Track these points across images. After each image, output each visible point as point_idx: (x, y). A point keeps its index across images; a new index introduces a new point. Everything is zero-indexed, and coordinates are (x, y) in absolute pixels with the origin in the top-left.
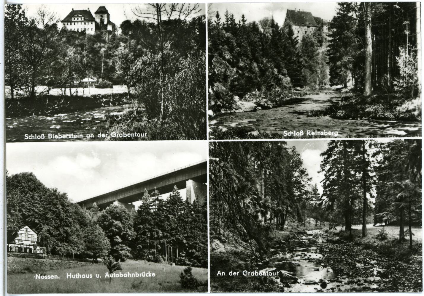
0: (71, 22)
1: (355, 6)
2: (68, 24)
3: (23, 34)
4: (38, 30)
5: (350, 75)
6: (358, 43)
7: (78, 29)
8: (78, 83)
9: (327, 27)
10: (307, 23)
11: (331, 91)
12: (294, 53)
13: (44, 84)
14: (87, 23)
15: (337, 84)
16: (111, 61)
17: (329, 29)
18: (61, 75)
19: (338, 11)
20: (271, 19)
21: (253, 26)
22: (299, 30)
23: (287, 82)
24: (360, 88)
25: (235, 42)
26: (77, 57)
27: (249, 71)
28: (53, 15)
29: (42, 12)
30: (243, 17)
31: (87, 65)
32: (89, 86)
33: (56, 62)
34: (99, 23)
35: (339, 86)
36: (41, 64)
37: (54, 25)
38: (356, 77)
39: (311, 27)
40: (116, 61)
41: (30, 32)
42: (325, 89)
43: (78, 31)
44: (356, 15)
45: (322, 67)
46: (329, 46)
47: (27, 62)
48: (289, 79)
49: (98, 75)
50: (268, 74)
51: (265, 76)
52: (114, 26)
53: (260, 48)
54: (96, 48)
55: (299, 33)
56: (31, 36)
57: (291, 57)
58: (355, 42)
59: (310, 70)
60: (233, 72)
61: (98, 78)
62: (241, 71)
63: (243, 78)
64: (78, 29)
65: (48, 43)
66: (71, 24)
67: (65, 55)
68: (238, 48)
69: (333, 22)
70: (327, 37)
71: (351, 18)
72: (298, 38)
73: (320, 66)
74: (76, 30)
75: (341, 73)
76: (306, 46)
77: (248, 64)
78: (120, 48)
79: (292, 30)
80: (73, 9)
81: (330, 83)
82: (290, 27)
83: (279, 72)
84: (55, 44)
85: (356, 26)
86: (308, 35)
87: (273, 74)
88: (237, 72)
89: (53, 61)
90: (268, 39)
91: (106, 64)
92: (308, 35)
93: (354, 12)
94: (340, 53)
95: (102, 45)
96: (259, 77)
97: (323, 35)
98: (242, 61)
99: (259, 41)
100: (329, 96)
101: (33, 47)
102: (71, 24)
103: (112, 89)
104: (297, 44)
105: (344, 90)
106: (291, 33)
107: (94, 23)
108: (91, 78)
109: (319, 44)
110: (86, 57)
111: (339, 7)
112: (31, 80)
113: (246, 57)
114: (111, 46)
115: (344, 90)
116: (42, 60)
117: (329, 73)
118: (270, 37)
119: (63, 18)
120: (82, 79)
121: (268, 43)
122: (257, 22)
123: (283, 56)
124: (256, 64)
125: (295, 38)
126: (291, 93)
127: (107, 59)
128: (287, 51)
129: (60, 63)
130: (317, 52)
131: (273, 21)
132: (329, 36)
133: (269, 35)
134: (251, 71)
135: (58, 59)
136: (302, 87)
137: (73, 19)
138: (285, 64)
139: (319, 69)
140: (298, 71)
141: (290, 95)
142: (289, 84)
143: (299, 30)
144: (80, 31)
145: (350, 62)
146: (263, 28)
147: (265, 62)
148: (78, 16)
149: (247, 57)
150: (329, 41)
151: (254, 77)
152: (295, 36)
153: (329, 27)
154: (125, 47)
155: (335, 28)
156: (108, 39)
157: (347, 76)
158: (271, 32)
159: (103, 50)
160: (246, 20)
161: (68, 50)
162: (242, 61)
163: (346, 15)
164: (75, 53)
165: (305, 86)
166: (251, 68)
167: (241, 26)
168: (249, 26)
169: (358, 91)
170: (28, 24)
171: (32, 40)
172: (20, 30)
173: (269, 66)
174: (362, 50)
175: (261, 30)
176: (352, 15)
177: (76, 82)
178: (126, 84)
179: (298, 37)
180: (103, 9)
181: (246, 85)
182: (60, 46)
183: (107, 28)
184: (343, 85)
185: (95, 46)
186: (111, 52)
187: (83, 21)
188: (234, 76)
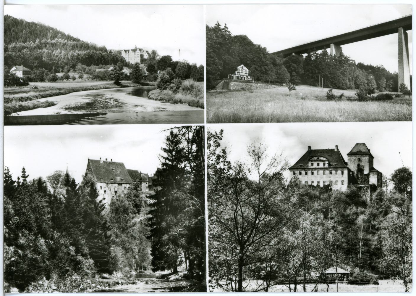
0: (306, 169)
1: (189, 153)
2: (300, 174)
3: (222, 190)
4: (249, 184)
5: (183, 255)
6: (194, 208)
7: (318, 182)
8: (318, 275)
9: (147, 185)
10: (118, 179)
11: (154, 279)
12: (99, 223)
13: (259, 278)
14: (334, 172)
15: (163, 269)
16: (376, 238)
17: (150, 187)
18: (288, 261)
19: (163, 161)
20: (65, 173)
21: (38, 183)
22: (106, 189)
23: (89, 266)
24: (198, 273)
25: (12, 208)
26: (317, 230)
27: (33, 250)
28: (276, 158)
29: (256, 152)
30: (24, 171)
31: (333, 245)
32: (336, 281)
33: (281, 240)
34: (355, 172)
35: (166, 272)
36: (253, 242)
37: (277, 176)
38: (191, 258)
39: (124, 185)
40: (384, 238)
41: (236, 187)
42: (145, 276)
43: (318, 186)
44: (191, 167)
45: (141, 244)
46: (151, 212)
47: (229, 239)
48: (92, 261)
49: (354, 262)
50: (60, 254)
51: (57, 258)
52: (380, 175)
53: (49, 216)
54: (349, 216)
55: (106, 194)
56: (237, 193)
57: (95, 230)
58: (189, 206)
59: (123, 248)
60: (10, 252)
61: (353, 268)
62: (21, 250)
63: (25, 261)
64: (318, 182)
65: (266, 206)
66: (306, 174)
67: (296, 227)
68: (17, 217)
69: (156, 177)
70: (148, 199)
71: (183, 169)
72: (104, 202)
73: (138, 242)
74: (315, 184)
75: (168, 253)
76: (116, 213)
77: (31, 240)
78: (390, 215)
79: (96, 189)
80: (310, 147)
81: (152, 267)
82: (93, 185)
83: (77, 251)
84: (279, 208)
85: (190, 183)
86: (119, 196)
87: (69, 254)
88: (16, 252)
89: (274, 237)
90: (61, 203)
91: (367, 242)
92: (119, 196)
93: (187, 162)
94: (166, 222)
95: (360, 209)
96: (48, 260)
97: (141, 196)
98: (22, 236)
99: (47, 206)
100: (151, 285)
101: (239, 212)
102: (306, 174)
103: (376, 286)
104: (103, 210)
105: (173, 277)
106: (94, 193)
107: (346, 172)
108: (341, 268)
109: (135, 210)
110: (332, 231)
111: (165, 155)
112: (235, 269)
113: (28, 230)
114: (375, 211)
115: (173, 277)
116: (255, 235)
117: (150, 252)
118: (63, 200)
119: (292, 162)
120: (325, 270)
121: (61, 209)
122: (44, 178)
123: (83, 228)
124: (43, 240)
125: (101, 202)
126: (95, 283)
127: (369, 233)
128: (88, 220)
129: (286, 241)
130: (133, 221)
131: (67, 175)
132: (151, 197)
133: (62, 197)
134: (36, 250)
135: (283, 233)
136: (111, 273)
137: (310, 164)
138: (86, 239)
139: (136, 247)
140: (105, 250)
141: (94, 285)
142: (92, 269)
143: (106, 189)
144: (322, 185)
145: (181, 235)
146: (54, 187)
147: (56, 237)
148: (318, 160)
149: (31, 230)
150: (150, 205)
151: (41, 260)
152: (98, 199)
153: (151, 184)
154: (399, 214)
155: (160, 185)
156: (371, 199)
157: (177, 256)
158: (65, 192)
159: (361, 218)
160: (28, 176)
161: (300, 219)
162: (22, 236)
163: (176, 166)
164: (312, 224)
165: (116, 271)
166: (37, 246)
167: (21, 184)
168: (33, 185)
169: (193, 278)
170: (231, 172)
171: (238, 200)
172: (217, 184)
173: (63, 242)
174: (199, 218)
175: (50, 189)
176: (185, 167)
177: (314, 274)
178: (401, 278)
179: (104, 199)
180: (363, 149)
181: (29, 271)
182: (287, 212)
183: (368, 181)
184: (172, 270)
185: (348, 211)
186: (376, 223)
187: (327, 169)
188: (11, 258)
